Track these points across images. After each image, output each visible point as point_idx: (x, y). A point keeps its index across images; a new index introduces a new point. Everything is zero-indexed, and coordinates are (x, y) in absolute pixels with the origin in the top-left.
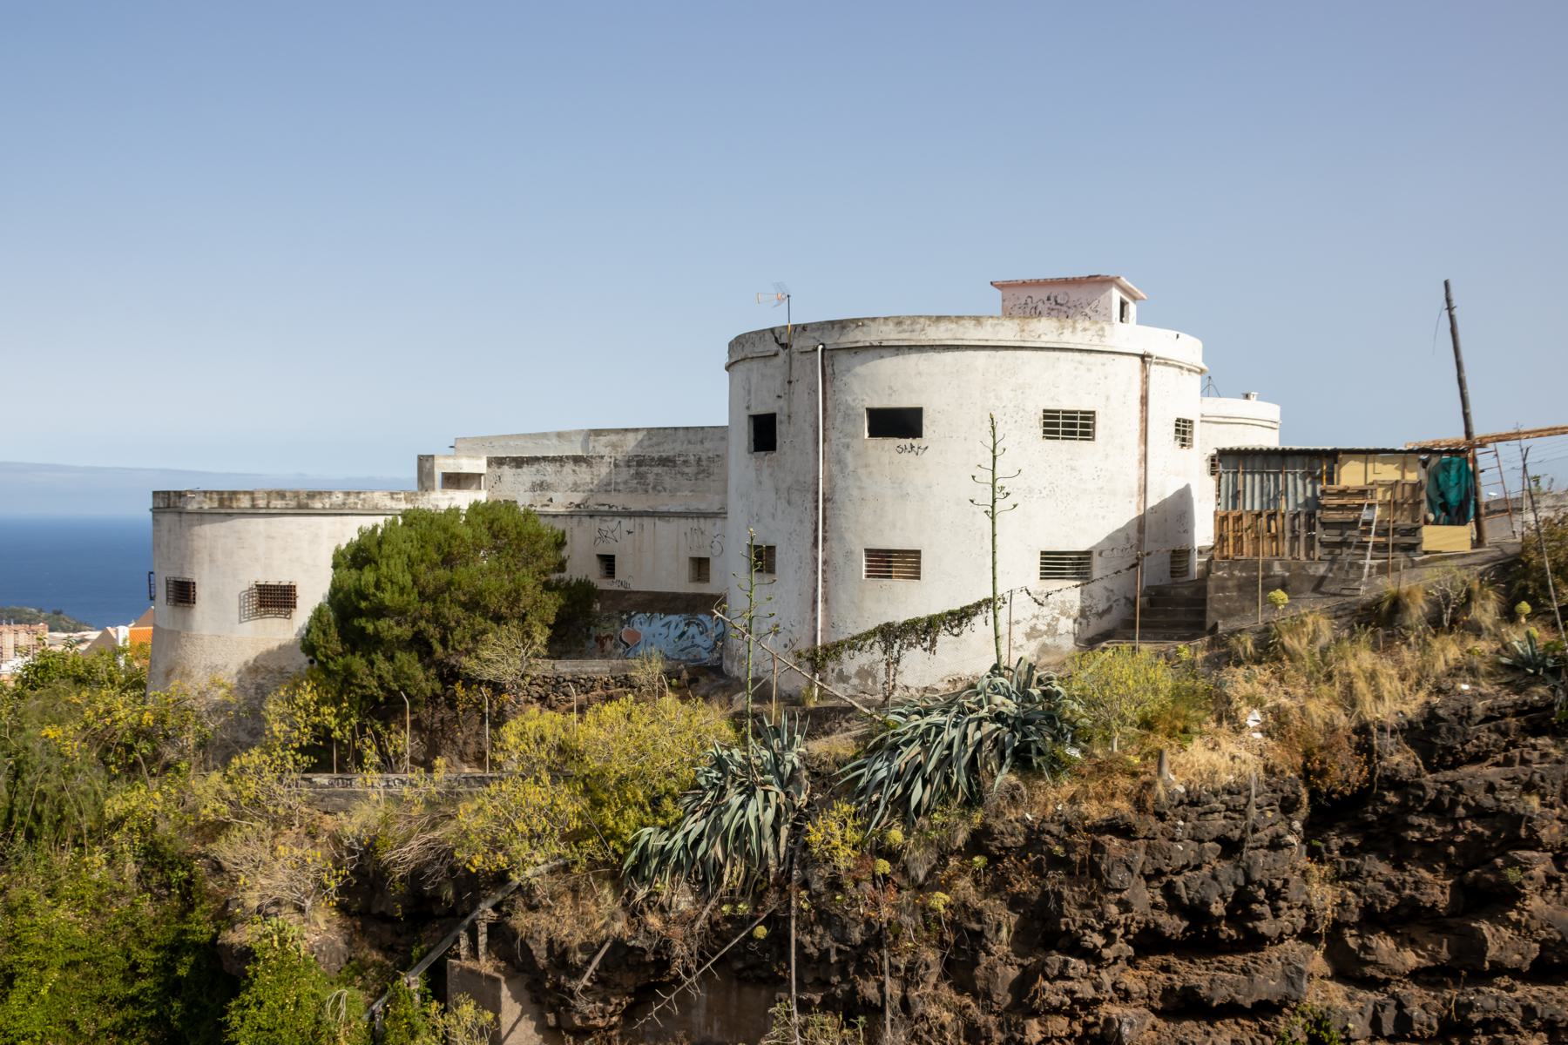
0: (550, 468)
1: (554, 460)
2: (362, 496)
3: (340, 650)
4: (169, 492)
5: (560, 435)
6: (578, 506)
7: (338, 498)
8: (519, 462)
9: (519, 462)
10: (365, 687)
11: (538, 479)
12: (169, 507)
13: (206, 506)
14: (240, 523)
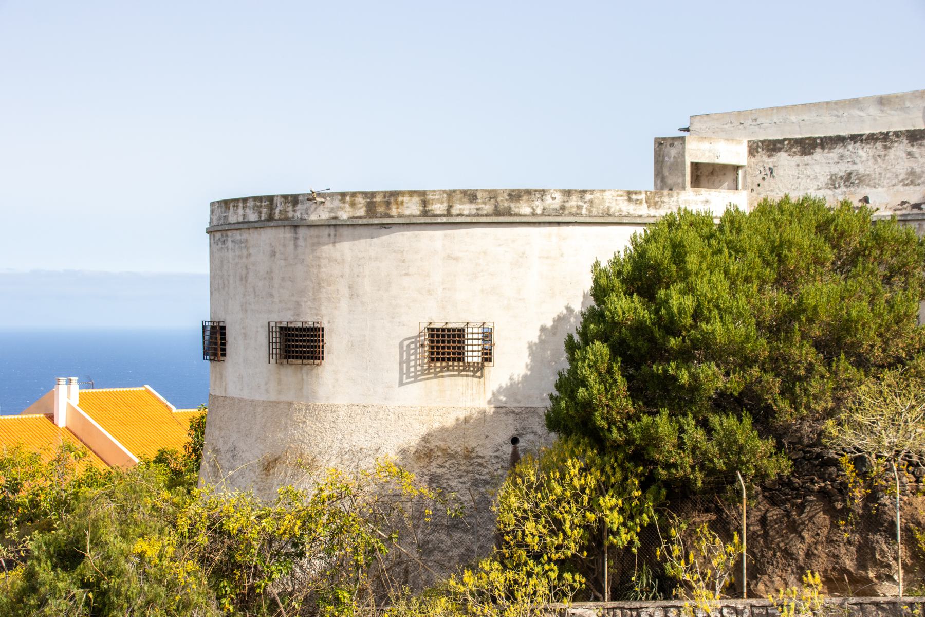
0: (864, 152)
1: (872, 138)
2: (588, 197)
3: (631, 409)
4: (271, 199)
5: (882, 101)
6: (917, 206)
7: (553, 201)
8: (806, 146)
9: (806, 146)
10: (675, 465)
11: (842, 169)
12: (271, 218)
13: (344, 215)
14: (402, 238)
